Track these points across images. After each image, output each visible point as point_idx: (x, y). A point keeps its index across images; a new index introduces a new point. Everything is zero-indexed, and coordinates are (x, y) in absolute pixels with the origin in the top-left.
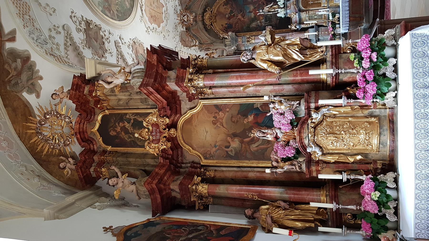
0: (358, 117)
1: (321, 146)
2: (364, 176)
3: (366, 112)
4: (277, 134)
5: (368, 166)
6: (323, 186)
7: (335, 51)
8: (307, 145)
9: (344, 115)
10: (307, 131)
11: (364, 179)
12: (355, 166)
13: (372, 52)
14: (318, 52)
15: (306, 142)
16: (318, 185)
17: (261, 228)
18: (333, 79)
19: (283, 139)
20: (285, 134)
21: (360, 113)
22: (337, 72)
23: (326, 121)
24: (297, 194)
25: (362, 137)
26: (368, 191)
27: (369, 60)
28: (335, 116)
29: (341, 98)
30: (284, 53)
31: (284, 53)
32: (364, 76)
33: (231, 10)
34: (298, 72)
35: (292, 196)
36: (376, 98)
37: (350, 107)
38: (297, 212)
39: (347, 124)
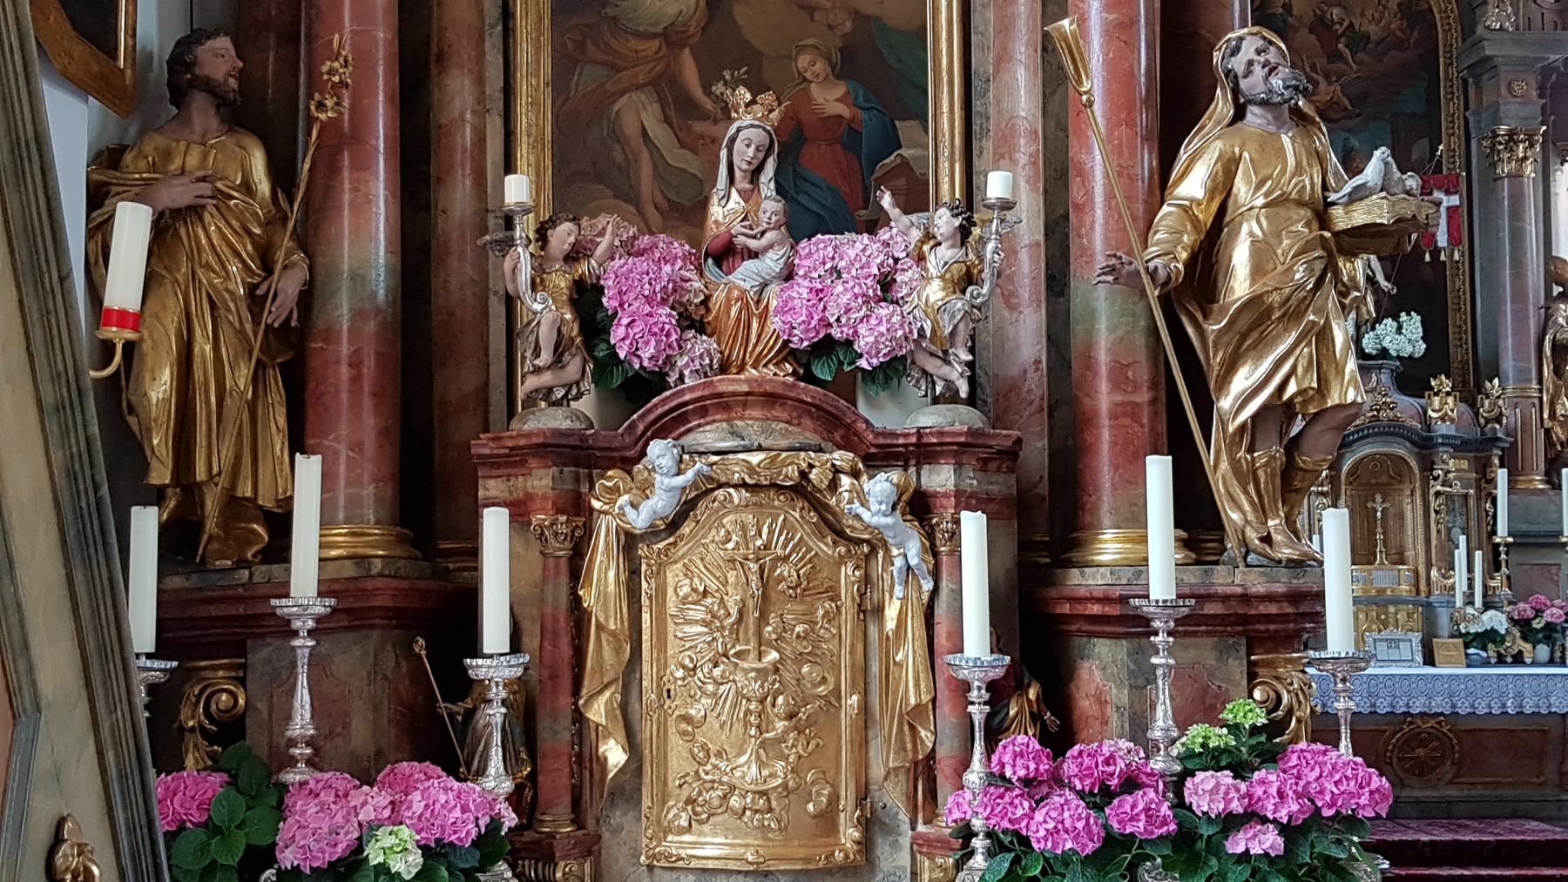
0: (862, 745)
1: (686, 529)
2: (507, 786)
3: (893, 797)
4: (754, 255)
5: (563, 808)
6: (414, 543)
7: (1268, 618)
8: (687, 440)
9: (875, 668)
10: (783, 443)
11: (489, 784)
12: (555, 734)
13: (1285, 830)
14: (1263, 512)
15: (710, 436)
16: (426, 510)
17: (111, 139)
18: (1105, 600)
19: (719, 296)
20: (754, 305)
21: (883, 760)
22: (1157, 624)
23: (842, 560)
24: (356, 380)
25: (746, 769)
26: (418, 807)
27: (1237, 807)
28: (869, 611)
29: (998, 646)
30: (1270, 309)
31: (1270, 309)
32: (1131, 783)
33: (1366, 37)
34: (1144, 396)
35: (345, 349)
36: (990, 854)
37: (926, 698)
38: (241, 377)
39: (824, 680)
